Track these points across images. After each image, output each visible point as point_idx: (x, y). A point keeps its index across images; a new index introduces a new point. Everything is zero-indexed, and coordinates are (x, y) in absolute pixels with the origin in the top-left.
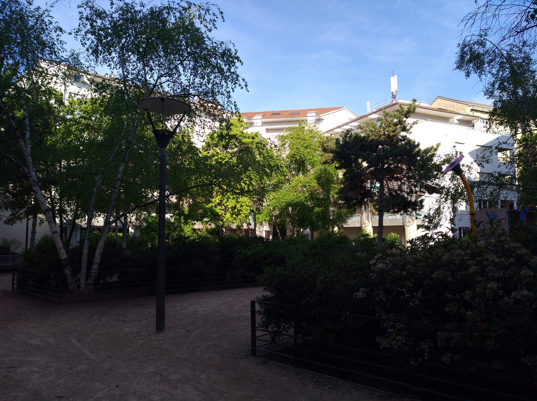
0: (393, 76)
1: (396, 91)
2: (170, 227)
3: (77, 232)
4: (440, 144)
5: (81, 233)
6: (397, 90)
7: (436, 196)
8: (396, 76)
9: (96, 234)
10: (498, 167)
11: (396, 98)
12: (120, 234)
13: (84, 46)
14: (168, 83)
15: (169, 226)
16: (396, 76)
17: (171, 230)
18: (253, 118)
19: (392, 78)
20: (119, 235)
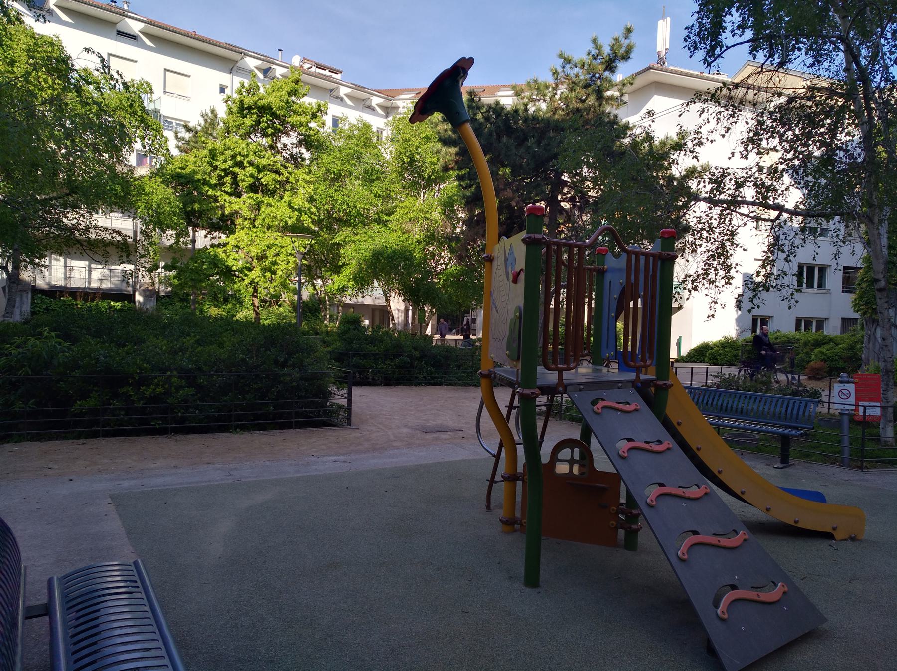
0: (663, 18)
1: (667, 49)
2: (216, 294)
3: (25, 298)
4: (470, 61)
5: (33, 298)
6: (668, 47)
7: (796, 283)
8: (669, 19)
9: (64, 301)
10: (729, 158)
11: (666, 63)
12: (117, 304)
13: (694, 95)
14: (315, 162)
15: (215, 292)
16: (669, 19)
17: (218, 301)
18: (396, 98)
19: (660, 23)
20: (114, 306)
